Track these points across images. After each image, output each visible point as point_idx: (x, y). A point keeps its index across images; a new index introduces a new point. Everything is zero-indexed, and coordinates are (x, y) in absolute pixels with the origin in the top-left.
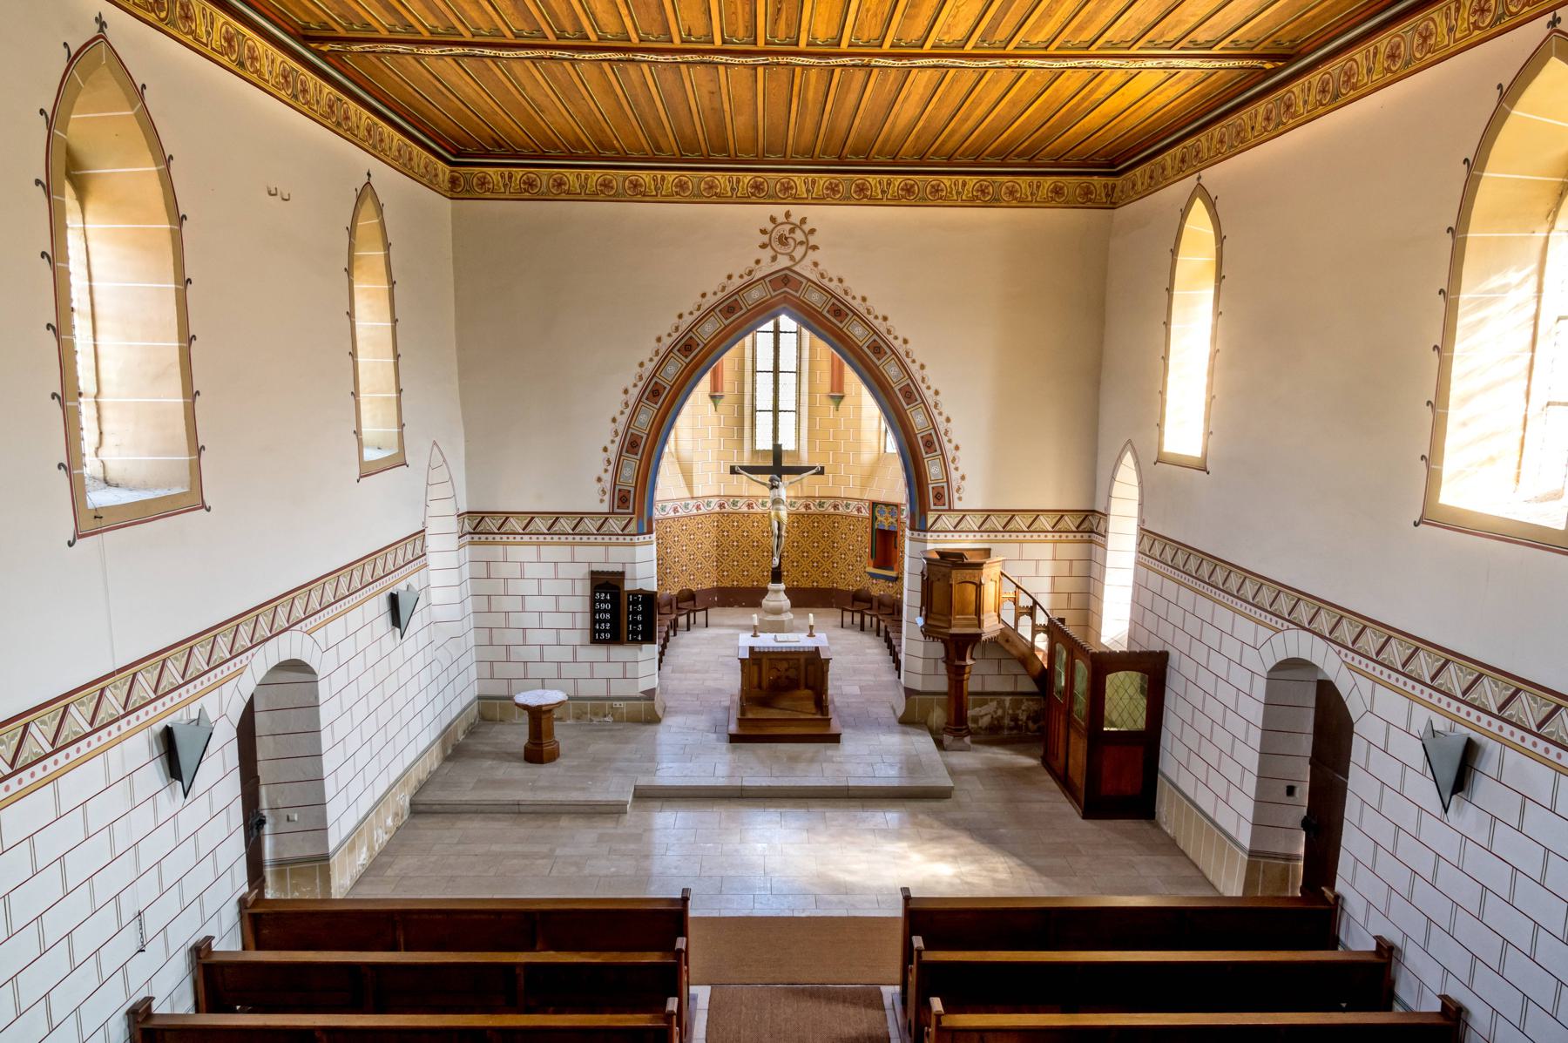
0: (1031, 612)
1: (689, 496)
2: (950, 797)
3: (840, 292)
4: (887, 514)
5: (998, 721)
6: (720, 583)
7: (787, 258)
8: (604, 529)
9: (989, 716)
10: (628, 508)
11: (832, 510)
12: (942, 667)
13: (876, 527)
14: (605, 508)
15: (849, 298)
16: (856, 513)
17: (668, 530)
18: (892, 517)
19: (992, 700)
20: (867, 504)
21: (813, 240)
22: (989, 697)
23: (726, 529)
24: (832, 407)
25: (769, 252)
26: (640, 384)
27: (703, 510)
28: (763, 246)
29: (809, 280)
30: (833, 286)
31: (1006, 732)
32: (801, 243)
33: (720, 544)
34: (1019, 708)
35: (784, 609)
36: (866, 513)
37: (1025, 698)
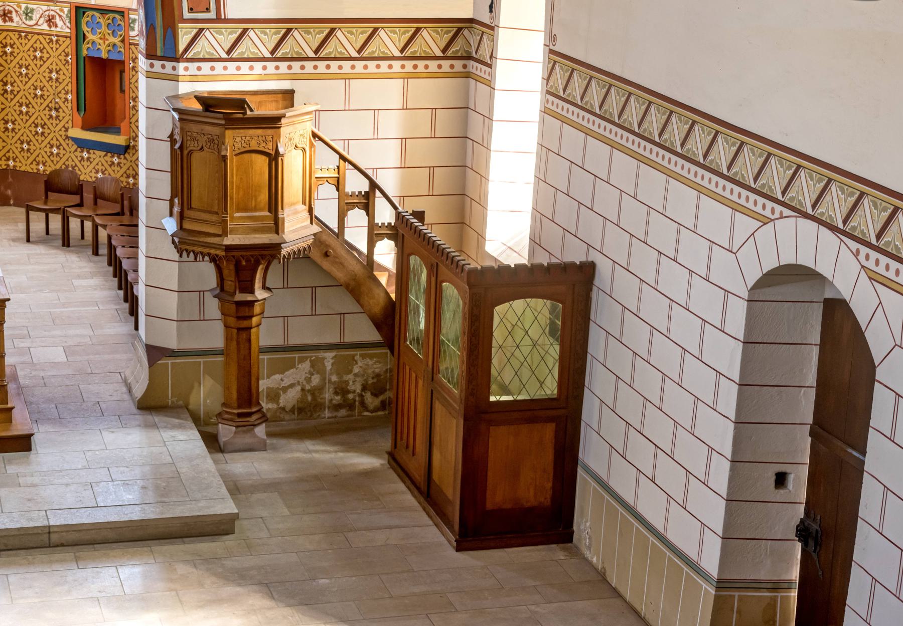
0: (366, 202)
4: (104, 29)
5: (313, 395)
9: (299, 388)
13: (85, 53)
16: (45, 27)
19: (302, 360)
20: (66, 10)
22: (296, 355)
31: (327, 414)
34: (350, 371)
36: (64, 27)
37: (358, 352)
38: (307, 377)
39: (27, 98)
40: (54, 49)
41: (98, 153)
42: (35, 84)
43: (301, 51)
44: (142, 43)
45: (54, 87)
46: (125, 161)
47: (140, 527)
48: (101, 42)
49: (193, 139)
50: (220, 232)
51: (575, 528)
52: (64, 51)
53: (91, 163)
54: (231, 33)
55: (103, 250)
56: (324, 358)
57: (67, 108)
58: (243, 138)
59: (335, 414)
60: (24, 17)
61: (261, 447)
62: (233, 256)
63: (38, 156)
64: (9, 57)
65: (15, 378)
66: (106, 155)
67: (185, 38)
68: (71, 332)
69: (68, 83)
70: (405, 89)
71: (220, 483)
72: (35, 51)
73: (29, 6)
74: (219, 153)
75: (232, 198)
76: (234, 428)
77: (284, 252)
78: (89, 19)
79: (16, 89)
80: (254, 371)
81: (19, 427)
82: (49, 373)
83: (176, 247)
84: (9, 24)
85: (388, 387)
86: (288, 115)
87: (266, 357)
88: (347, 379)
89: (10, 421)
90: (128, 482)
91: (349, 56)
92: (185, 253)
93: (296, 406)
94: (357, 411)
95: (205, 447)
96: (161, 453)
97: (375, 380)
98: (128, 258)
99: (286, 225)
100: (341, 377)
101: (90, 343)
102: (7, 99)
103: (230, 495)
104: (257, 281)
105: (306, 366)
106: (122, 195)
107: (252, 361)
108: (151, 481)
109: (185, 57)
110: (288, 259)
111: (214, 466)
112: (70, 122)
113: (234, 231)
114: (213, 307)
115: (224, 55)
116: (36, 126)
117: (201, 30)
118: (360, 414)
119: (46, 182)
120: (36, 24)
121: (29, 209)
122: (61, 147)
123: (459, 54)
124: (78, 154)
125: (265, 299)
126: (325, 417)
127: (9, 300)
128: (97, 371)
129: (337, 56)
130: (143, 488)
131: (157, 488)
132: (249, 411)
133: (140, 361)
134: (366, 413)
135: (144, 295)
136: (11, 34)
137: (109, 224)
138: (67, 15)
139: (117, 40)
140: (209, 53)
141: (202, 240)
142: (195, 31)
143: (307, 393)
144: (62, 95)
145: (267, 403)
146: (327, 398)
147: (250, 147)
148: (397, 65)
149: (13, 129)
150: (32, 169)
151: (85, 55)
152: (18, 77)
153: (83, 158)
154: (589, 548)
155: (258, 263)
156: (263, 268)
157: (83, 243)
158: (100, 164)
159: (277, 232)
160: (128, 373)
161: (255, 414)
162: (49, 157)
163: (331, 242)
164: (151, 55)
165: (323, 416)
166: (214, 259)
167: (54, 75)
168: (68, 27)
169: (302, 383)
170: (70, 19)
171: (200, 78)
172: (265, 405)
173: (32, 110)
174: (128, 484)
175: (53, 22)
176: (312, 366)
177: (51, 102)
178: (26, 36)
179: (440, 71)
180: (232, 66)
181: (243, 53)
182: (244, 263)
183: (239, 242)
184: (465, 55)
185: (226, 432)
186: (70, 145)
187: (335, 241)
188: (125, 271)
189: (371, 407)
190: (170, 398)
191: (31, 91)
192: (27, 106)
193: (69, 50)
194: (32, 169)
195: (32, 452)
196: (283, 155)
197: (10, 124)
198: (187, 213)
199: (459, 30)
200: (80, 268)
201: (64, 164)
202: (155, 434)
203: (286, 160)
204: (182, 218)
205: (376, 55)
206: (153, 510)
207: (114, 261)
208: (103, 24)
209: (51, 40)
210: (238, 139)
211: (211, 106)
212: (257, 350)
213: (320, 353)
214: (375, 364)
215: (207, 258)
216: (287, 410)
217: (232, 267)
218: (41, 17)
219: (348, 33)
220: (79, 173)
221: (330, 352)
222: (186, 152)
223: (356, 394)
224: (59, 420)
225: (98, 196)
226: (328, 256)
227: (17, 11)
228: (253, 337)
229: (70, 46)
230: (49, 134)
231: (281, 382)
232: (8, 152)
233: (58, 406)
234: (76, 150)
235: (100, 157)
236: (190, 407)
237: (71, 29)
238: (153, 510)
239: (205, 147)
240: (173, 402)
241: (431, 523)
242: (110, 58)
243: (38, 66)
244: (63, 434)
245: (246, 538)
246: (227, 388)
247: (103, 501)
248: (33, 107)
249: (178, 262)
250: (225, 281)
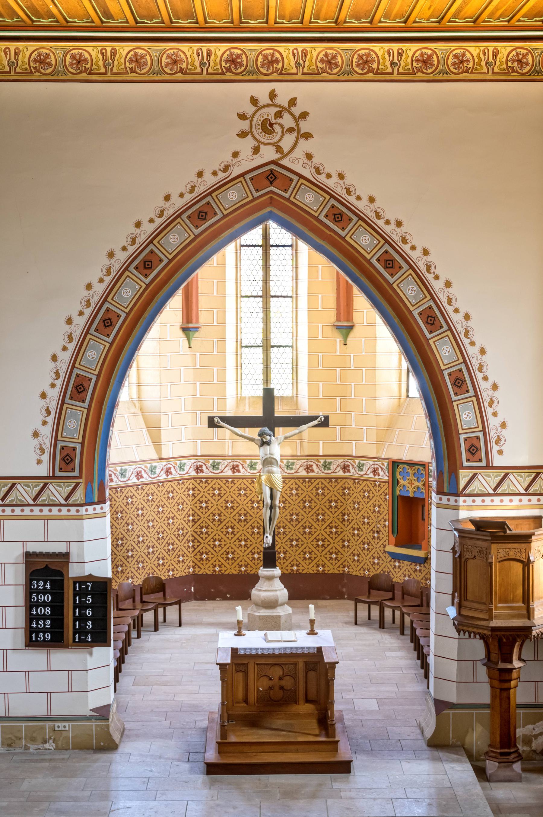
1: (156, 456)
3: (340, 191)
4: (411, 476)
6: (197, 569)
7: (272, 149)
8: (43, 498)
10: (73, 470)
11: (341, 473)
13: (398, 493)
14: (43, 470)
15: (352, 199)
16: (371, 475)
17: (130, 500)
18: (418, 480)
20: (386, 464)
21: (305, 126)
23: (204, 499)
24: (338, 340)
25: (249, 143)
26: (88, 312)
27: (175, 475)
28: (243, 135)
29: (301, 176)
30: (330, 183)
32: (291, 130)
33: (196, 518)
35: (280, 601)
36: (384, 475)
39: (358, 525)
40: (377, 491)
41: (406, 563)
42: (364, 515)
44: (434, 484)
45: (376, 517)
46: (424, 569)
48: (409, 485)
49: (468, 550)
50: (487, 617)
52: (384, 492)
53: (401, 569)
54: (496, 476)
55: (408, 631)
57: (386, 533)
58: (504, 550)
60: (357, 469)
61: (517, 779)
62: (497, 635)
63: (364, 565)
64: (346, 496)
65: (341, 720)
66: (411, 564)
68: (383, 689)
73: (361, 461)
74: (487, 560)
75: (496, 593)
76: (497, 764)
77: (534, 633)
78: (401, 470)
79: (351, 518)
80: (512, 721)
81: (343, 755)
82: (366, 718)
83: (456, 628)
84: (347, 474)
86: (536, 533)
87: (521, 711)
89: (336, 750)
92: (462, 633)
95: (475, 777)
98: (424, 637)
99: (536, 613)
101: (396, 697)
102: (344, 525)
103: (494, 814)
104: (514, 654)
106: (422, 592)
110: (537, 638)
111: (482, 792)
112: (387, 541)
113: (497, 617)
114: (482, 672)
115: (491, 492)
116: (364, 544)
117: (475, 474)
119: (369, 582)
121: (357, 601)
124: (392, 563)
125: (520, 668)
127: (338, 663)
128: (400, 718)
130: (430, 804)
131: (439, 805)
133: (430, 711)
135: (433, 662)
136: (348, 480)
137: (411, 613)
138: (386, 467)
139: (420, 484)
140: (481, 490)
141: (474, 622)
142: (471, 475)
144: (382, 523)
145: (522, 747)
149: (348, 546)
150: (339, 571)
152: (352, 510)
153: (395, 566)
155: (514, 642)
156: (518, 645)
157: (394, 626)
158: (407, 570)
159: (529, 619)
160: (421, 720)
162: (372, 565)
164: (440, 492)
166: (482, 637)
167: (377, 509)
170: (388, 470)
171: (474, 508)
172: (521, 748)
173: (361, 533)
174: (418, 801)
177: (374, 527)
178: (358, 482)
180: (497, 499)
181: (505, 490)
182: (505, 640)
185: (491, 766)
186: (387, 557)
188: (422, 646)
191: (361, 520)
192: (358, 530)
194: (339, 571)
195: (352, 774)
196: (533, 563)
197: (346, 542)
200: (391, 643)
201: (382, 570)
202: (439, 766)
203: (535, 565)
204: (460, 607)
207: (415, 639)
208: (411, 473)
209: (375, 485)
210: (501, 551)
211: (481, 527)
212: (514, 705)
215: (478, 637)
217: (496, 643)
218: (369, 469)
220: (392, 577)
222: (463, 560)
224: (371, 752)
225: (405, 593)
227: (353, 465)
228: (512, 696)
230: (372, 549)
232: (345, 561)
233: (371, 741)
234: (391, 561)
236: (465, 746)
239: (476, 556)
240: (453, 742)
242: (416, 496)
243: (366, 502)
244: (374, 762)
246: (492, 733)
247: (400, 813)
248: (362, 531)
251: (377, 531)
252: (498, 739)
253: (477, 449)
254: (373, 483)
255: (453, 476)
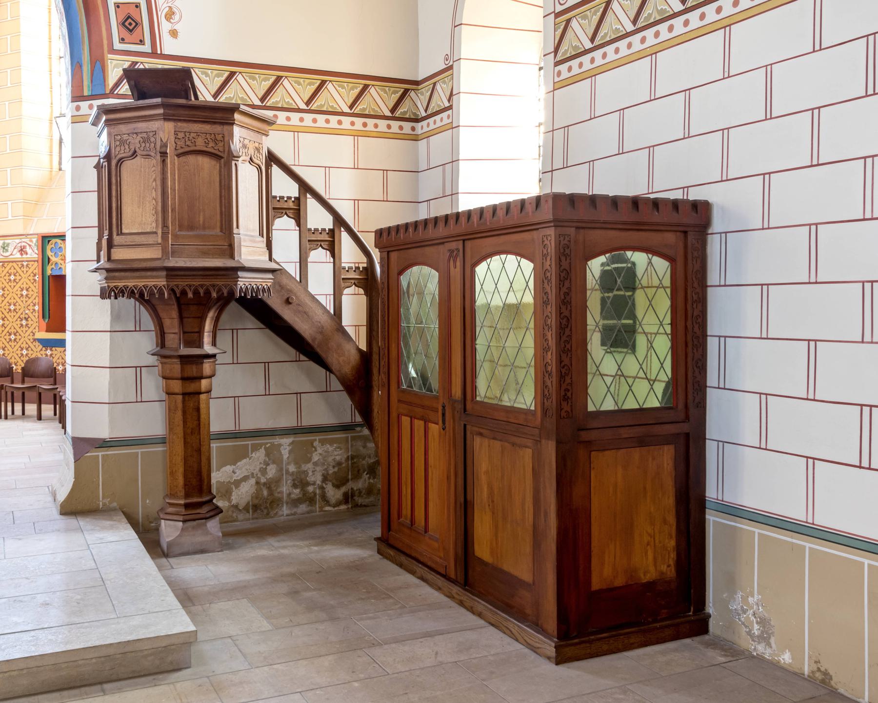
2: (189, 667)
5: (269, 488)
9: (253, 481)
12: (153, 386)
16: (18, 255)
19: (255, 448)
20: (34, 240)
22: (249, 442)
31: (285, 510)
34: (309, 460)
36: (33, 253)
37: (317, 437)
38: (262, 468)
40: (25, 272)
43: (246, 97)
45: (24, 302)
47: (25, 671)
51: (710, 608)
52: (32, 272)
56: (280, 445)
58: (187, 134)
59: (295, 510)
67: (116, 71)
69: (36, 297)
70: (356, 147)
71: (165, 588)
72: (10, 275)
76: (181, 524)
85: (350, 477)
88: (306, 469)
90: (21, 598)
91: (297, 107)
93: (251, 503)
94: (317, 506)
96: (81, 558)
97: (336, 469)
100: (300, 467)
105: (260, 455)
107: (201, 436)
108: (58, 593)
109: (115, 93)
112: (37, 328)
116: (10, 334)
118: (321, 508)
120: (11, 255)
122: (30, 349)
123: (407, 116)
126: (283, 515)
129: (284, 107)
132: (200, 500)
133: (67, 465)
134: (327, 508)
143: (262, 487)
144: (31, 308)
146: (285, 491)
147: (195, 146)
148: (346, 120)
151: (49, 274)
154: (764, 638)
156: (212, 318)
158: (60, 358)
161: (206, 505)
163: (293, 286)
165: (281, 513)
167: (25, 293)
168: (36, 253)
169: (257, 475)
170: (38, 247)
175: (24, 251)
176: (267, 455)
179: (389, 131)
183: (184, 264)
184: (412, 117)
186: (37, 346)
187: (297, 285)
189: (333, 501)
190: (101, 500)
193: (36, 271)
198: (117, 239)
199: (406, 91)
205: (325, 109)
206: (53, 637)
209: (23, 265)
213: (276, 439)
214: (336, 451)
216: (241, 508)
218: (15, 248)
219: (295, 83)
221: (287, 438)
223: (316, 486)
226: (290, 303)
229: (37, 268)
231: (233, 474)
234: (41, 350)
235: (61, 352)
237: (38, 254)
238: (53, 637)
240: (104, 504)
241: (482, 622)
243: (12, 287)
245: (210, 674)
248: (8, 320)
249: (110, 331)
250: (166, 335)
251: (25, 318)
252: (181, 480)
253: (137, 24)
254: (19, 263)
255: (98, 65)
